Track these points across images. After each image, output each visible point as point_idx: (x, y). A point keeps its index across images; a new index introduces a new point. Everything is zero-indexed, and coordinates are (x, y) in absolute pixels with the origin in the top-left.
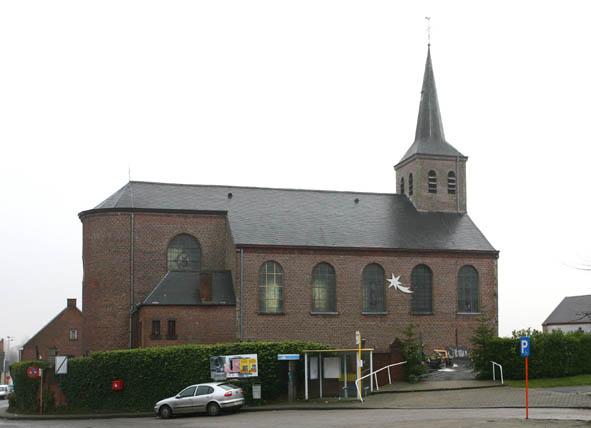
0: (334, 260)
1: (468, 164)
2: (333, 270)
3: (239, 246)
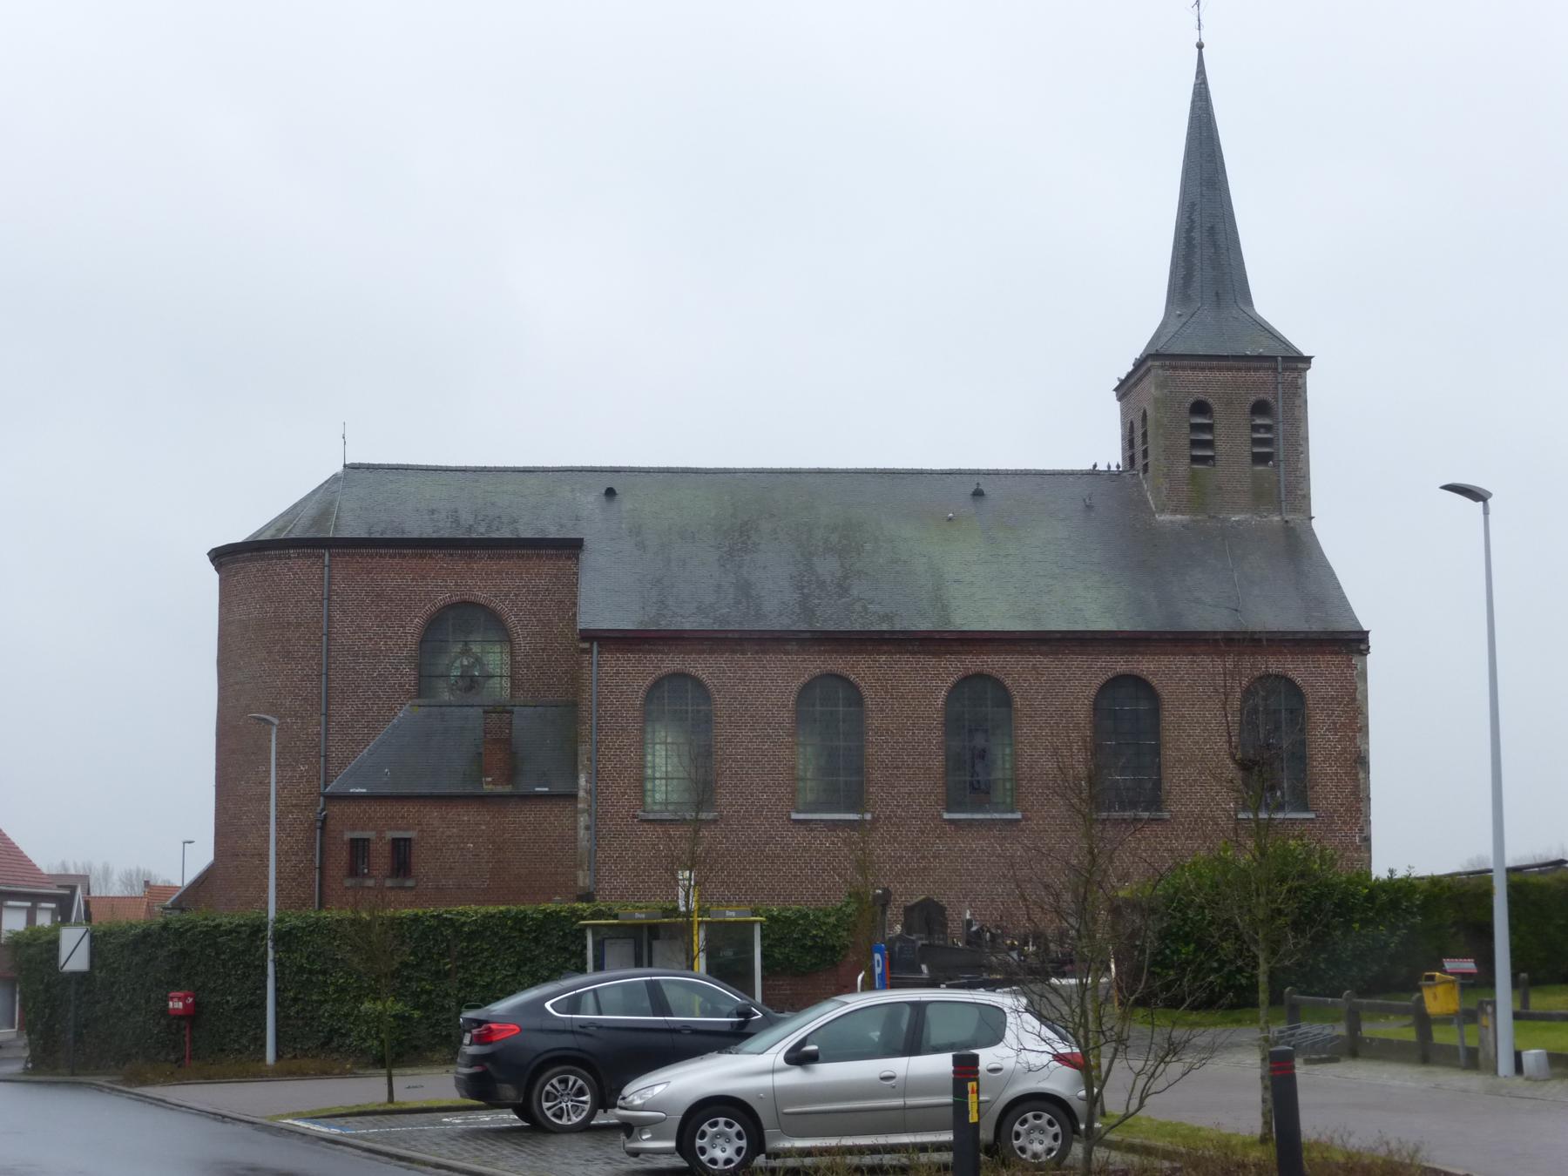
0: (861, 668)
1: (1311, 376)
2: (855, 696)
3: (589, 636)
